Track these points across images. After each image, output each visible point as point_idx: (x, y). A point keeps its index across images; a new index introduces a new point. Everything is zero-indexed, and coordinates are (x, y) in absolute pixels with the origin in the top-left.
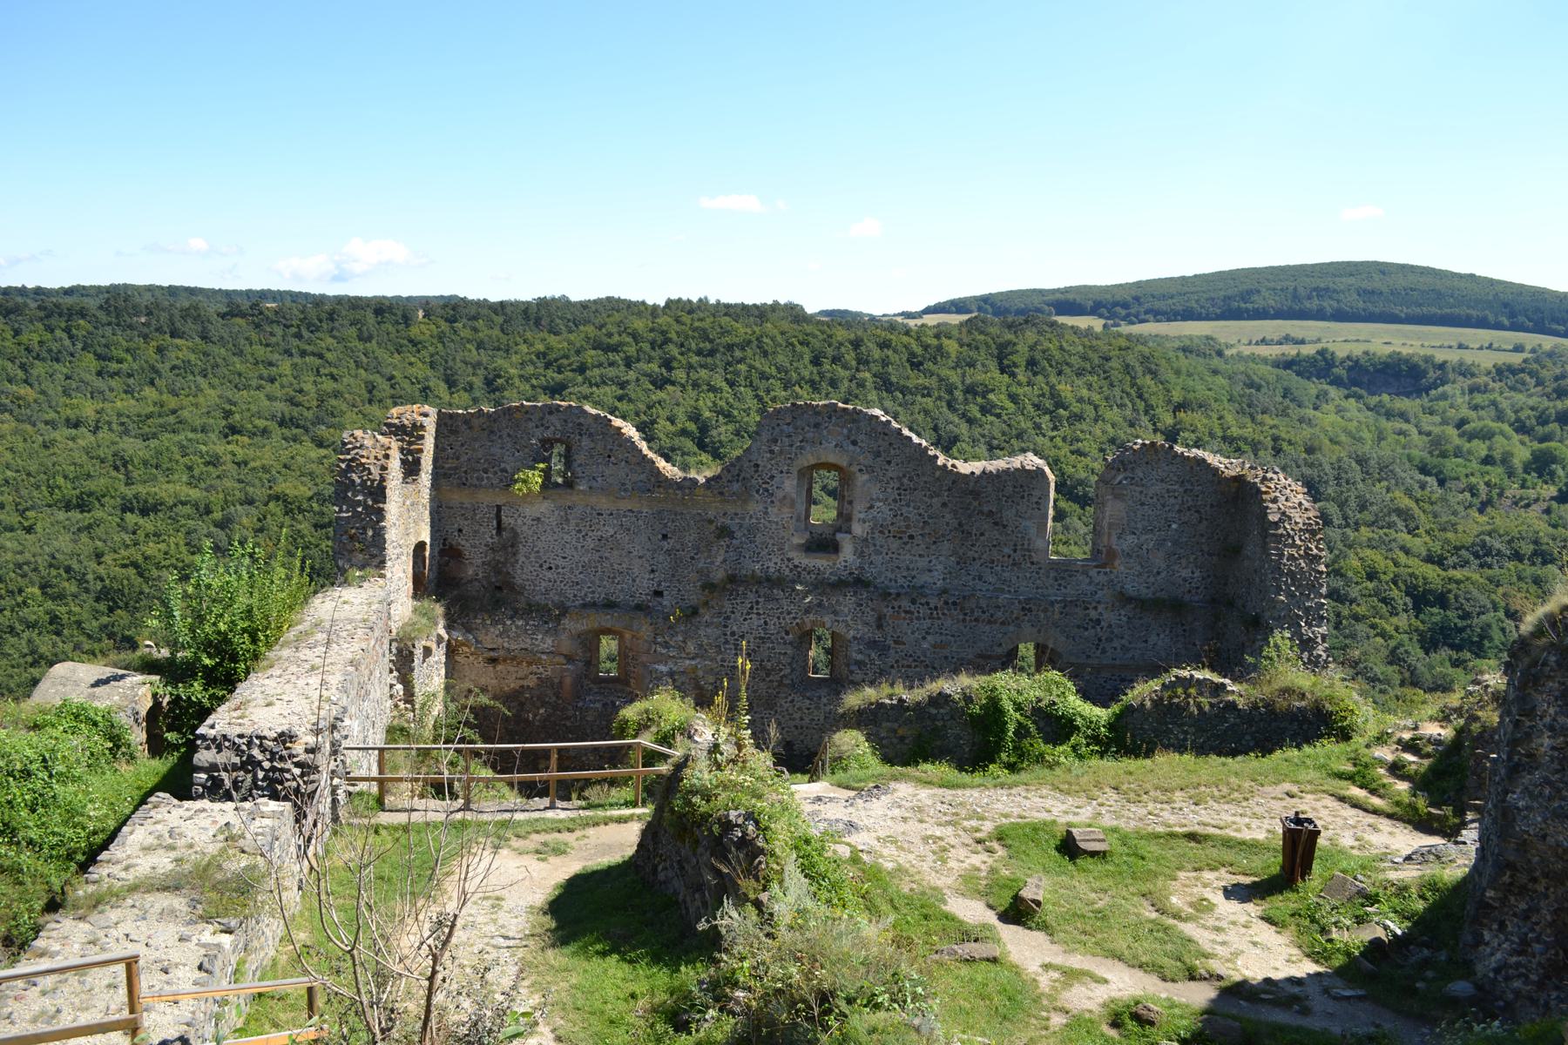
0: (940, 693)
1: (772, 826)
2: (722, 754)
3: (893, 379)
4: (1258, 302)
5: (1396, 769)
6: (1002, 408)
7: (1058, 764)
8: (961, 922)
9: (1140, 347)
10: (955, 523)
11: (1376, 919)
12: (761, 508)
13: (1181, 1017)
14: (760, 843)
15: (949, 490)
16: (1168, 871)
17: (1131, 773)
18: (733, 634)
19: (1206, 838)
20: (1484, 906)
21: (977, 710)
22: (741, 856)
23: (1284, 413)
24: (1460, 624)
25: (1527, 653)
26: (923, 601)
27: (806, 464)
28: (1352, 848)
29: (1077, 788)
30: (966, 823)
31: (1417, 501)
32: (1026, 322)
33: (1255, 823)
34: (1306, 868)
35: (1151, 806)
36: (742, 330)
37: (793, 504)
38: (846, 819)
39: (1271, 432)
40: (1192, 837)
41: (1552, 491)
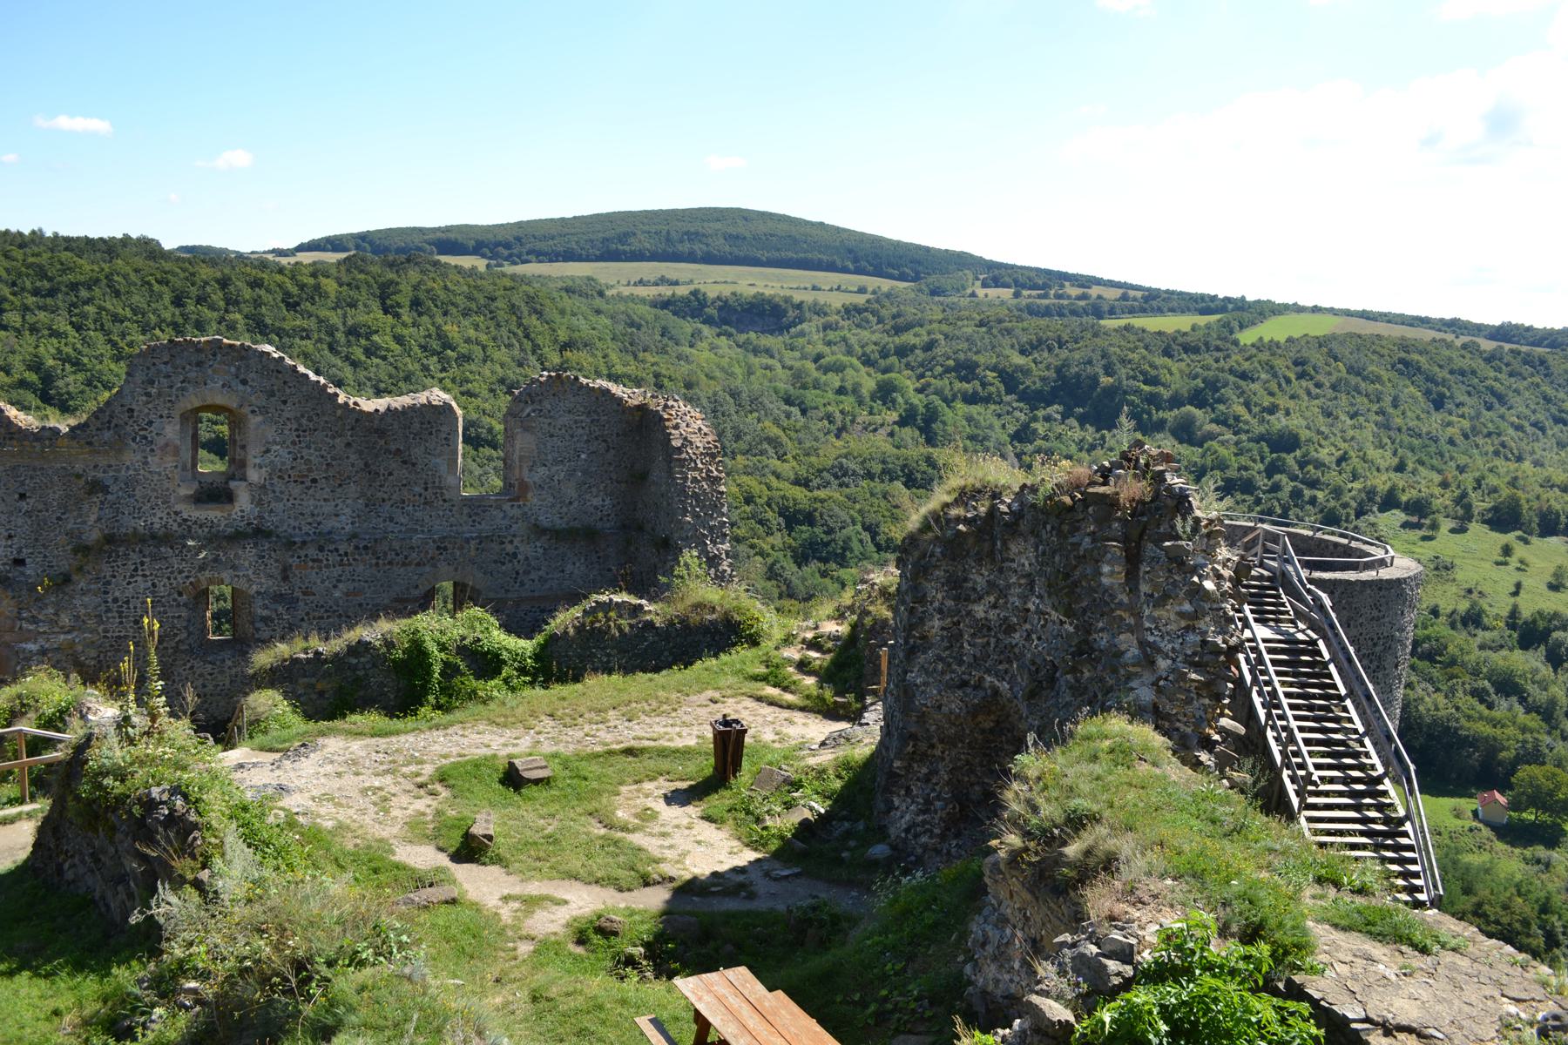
0: (359, 642)
1: (205, 797)
2: (133, 727)
3: (268, 321)
4: (635, 245)
5: (803, 666)
6: (388, 350)
7: (491, 698)
8: (413, 870)
9: (525, 288)
10: (361, 464)
11: (802, 802)
12: (139, 457)
13: (642, 922)
14: (193, 817)
15: (352, 429)
16: (610, 788)
17: (564, 699)
18: (115, 600)
19: (643, 751)
20: (892, 775)
21: (400, 655)
22: (172, 835)
23: (663, 351)
24: (826, 538)
25: (917, 547)
26: (332, 547)
27: (189, 407)
28: (774, 742)
29: (513, 720)
30: (404, 770)
31: (784, 430)
32: (408, 261)
33: (685, 731)
34: (737, 766)
35: (587, 728)
36: (88, 267)
37: (176, 451)
38: (275, 783)
39: (653, 369)
40: (629, 752)
41: (895, 416)
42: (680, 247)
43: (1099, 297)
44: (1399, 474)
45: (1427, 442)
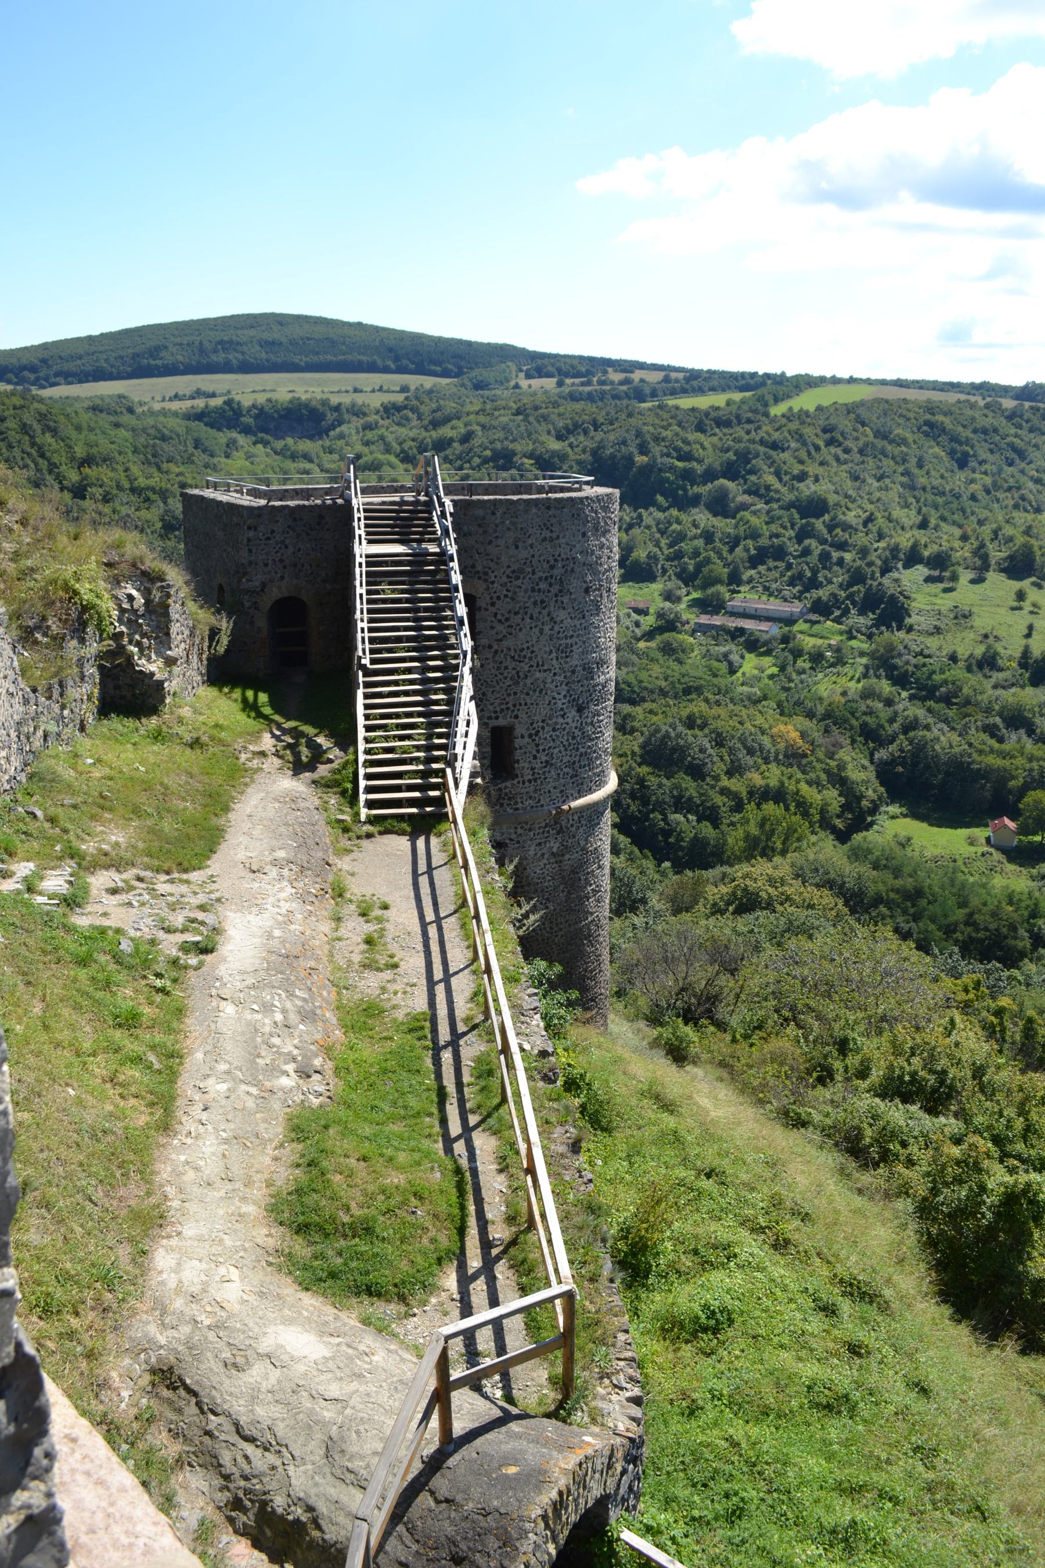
4: (167, 358)
9: (36, 405)
42: (214, 358)
43: (642, 380)
44: (922, 532)
45: (950, 499)
